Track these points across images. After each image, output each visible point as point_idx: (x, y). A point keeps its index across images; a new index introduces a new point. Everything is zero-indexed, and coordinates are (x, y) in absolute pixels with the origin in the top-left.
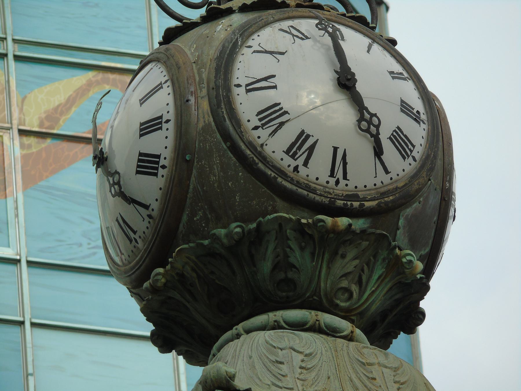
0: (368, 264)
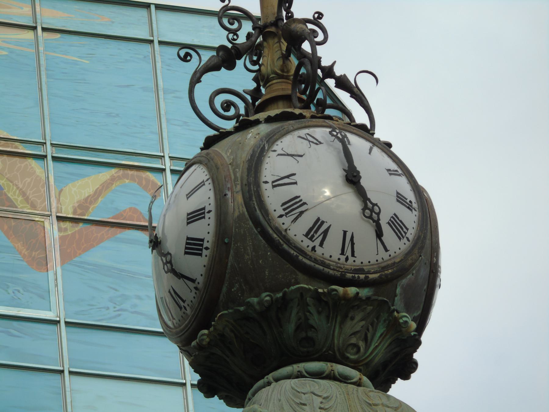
0: (372, 324)
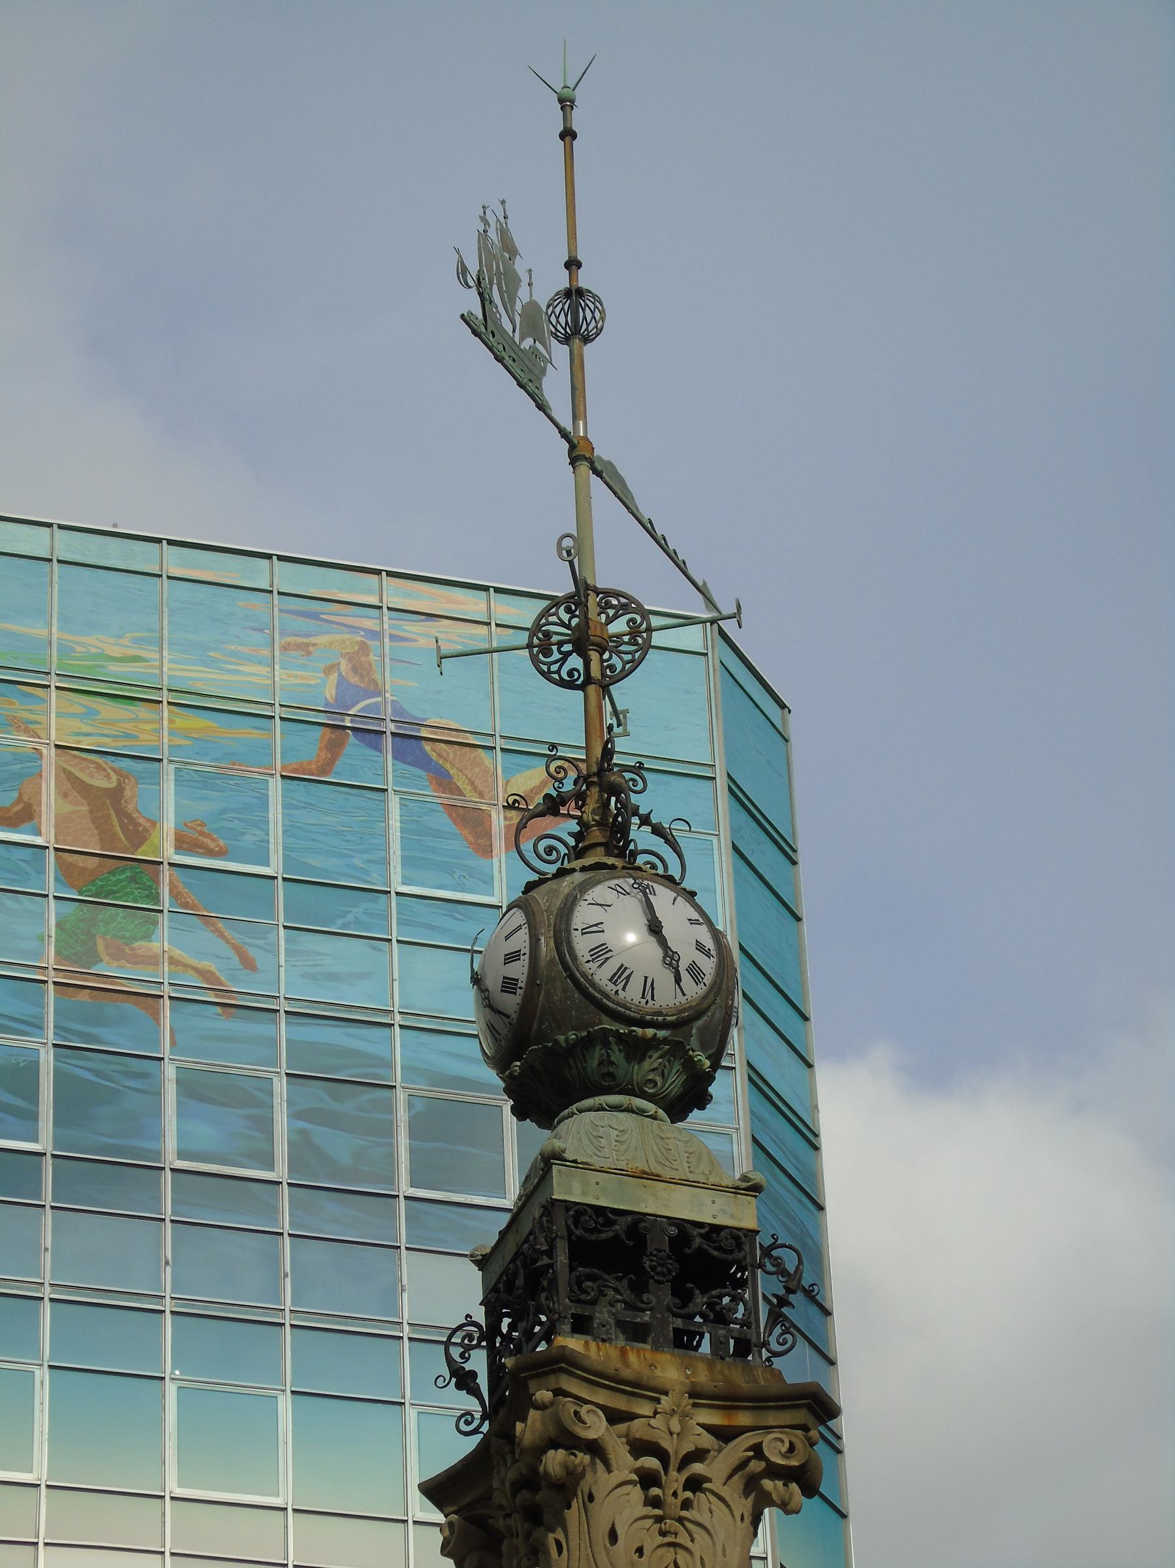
0: (669, 1062)
